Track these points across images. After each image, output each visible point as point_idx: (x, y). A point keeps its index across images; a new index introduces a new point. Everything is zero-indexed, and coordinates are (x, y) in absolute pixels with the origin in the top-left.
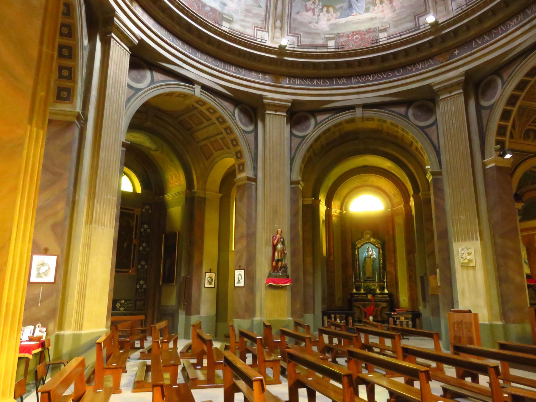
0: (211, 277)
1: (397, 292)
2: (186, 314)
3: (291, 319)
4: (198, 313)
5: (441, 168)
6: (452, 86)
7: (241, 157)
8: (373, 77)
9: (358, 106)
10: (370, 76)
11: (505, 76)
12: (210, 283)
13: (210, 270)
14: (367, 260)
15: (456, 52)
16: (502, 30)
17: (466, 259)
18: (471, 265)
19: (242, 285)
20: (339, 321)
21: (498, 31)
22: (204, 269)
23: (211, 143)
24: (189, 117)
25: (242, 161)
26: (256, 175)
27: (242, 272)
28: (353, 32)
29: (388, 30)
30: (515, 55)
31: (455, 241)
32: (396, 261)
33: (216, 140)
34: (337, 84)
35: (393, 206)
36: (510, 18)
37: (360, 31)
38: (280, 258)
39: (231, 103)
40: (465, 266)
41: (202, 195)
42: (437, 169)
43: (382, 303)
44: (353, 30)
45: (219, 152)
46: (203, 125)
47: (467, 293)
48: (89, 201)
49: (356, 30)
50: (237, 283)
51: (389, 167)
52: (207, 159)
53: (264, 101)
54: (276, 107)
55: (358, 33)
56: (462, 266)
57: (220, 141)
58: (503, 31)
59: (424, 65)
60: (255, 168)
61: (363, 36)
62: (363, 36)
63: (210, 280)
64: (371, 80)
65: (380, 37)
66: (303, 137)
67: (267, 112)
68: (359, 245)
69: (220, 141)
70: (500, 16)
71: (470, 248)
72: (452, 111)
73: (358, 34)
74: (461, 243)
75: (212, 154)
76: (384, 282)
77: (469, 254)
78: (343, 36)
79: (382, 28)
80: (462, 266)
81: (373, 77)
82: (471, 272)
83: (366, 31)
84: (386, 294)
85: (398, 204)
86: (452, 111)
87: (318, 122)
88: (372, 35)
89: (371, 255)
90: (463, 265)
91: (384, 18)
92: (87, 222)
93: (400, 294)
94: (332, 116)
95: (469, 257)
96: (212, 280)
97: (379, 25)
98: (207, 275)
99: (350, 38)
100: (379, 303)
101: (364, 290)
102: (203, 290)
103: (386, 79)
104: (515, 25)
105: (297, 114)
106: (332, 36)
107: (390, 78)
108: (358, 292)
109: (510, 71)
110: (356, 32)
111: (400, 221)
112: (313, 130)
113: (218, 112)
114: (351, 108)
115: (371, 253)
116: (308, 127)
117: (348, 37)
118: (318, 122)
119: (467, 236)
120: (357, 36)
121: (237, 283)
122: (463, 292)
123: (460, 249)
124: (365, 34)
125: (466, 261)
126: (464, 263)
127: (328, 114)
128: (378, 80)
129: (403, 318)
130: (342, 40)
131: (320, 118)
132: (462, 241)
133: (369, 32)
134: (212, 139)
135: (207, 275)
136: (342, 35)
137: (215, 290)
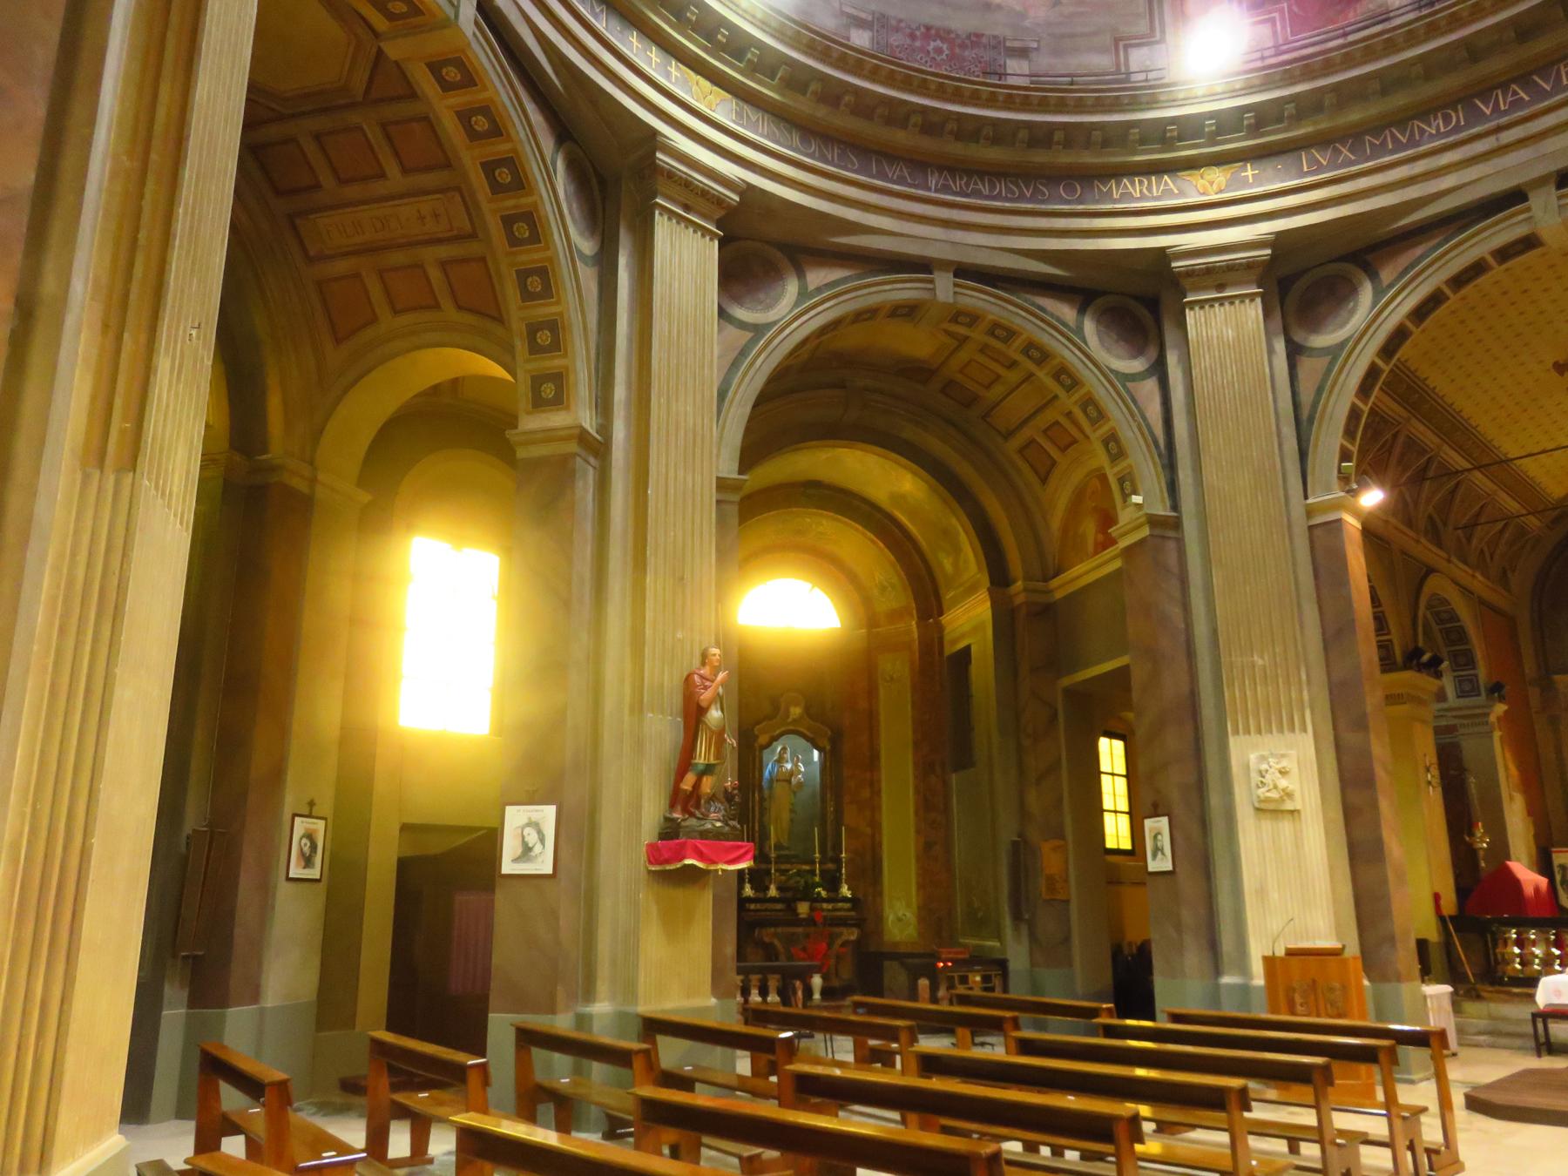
0: (310, 836)
1: (879, 894)
2: (194, 1002)
3: (713, 1001)
4: (254, 995)
5: (1175, 506)
6: (1231, 268)
7: (556, 346)
8: (993, 187)
9: (944, 265)
10: (983, 181)
11: (1386, 275)
12: (308, 861)
13: (311, 804)
14: (779, 789)
15: (1249, 173)
16: (1395, 139)
17: (1275, 787)
18: (1289, 806)
19: (543, 864)
20: (759, 999)
21: (1384, 143)
22: (290, 802)
23: (381, 274)
24: (318, 137)
25: (557, 362)
26: (606, 429)
27: (547, 814)
28: (928, 28)
29: (1033, 55)
30: (1436, 215)
31: (1236, 732)
32: (877, 793)
33: (420, 266)
34: (882, 175)
35: (871, 622)
36: (1425, 112)
37: (949, 32)
38: (712, 761)
39: (547, 119)
40: (1270, 810)
41: (298, 483)
42: (1161, 509)
43: (844, 930)
44: (927, 20)
45: (406, 319)
46: (380, 188)
47: (1274, 896)
48: (113, 328)
49: (938, 23)
50: (516, 860)
51: (899, 499)
52: (338, 341)
53: (1174, 265)
54: (1218, 276)
55: (944, 34)
56: (1258, 810)
57: (435, 274)
58: (1399, 147)
59: (1149, 189)
60: (604, 406)
61: (957, 50)
62: (957, 50)
63: (306, 849)
64: (986, 192)
65: (1009, 71)
66: (758, 330)
67: (658, 200)
68: (763, 739)
69: (435, 274)
70: (1399, 100)
71: (1283, 756)
72: (1226, 334)
73: (943, 39)
74: (1254, 737)
75: (374, 320)
76: (813, 862)
77: (1283, 773)
78: (897, 30)
79: (1016, 44)
80: (1258, 810)
81: (993, 187)
82: (1286, 826)
83: (969, 37)
84: (845, 899)
85: (894, 616)
86: (1226, 334)
87: (811, 287)
88: (987, 56)
89: (791, 773)
90: (1263, 806)
91: (1023, 16)
92: (95, 455)
93: (886, 899)
94: (859, 277)
95: (1283, 783)
96: (314, 847)
97: (1008, 33)
98: (301, 825)
99: (918, 44)
100: (836, 930)
101: (779, 889)
102: (283, 890)
103: (1030, 201)
104: (1439, 135)
105: (756, 245)
106: (863, 15)
107: (1043, 202)
108: (761, 895)
109: (1404, 260)
110: (938, 30)
111: (897, 669)
112: (792, 310)
113: (509, 139)
114: (921, 266)
115: (789, 766)
116: (777, 300)
117: (913, 36)
118: (811, 287)
119: (1278, 719)
120: (938, 43)
121: (516, 860)
122: (1262, 892)
123: (1253, 757)
124: (963, 46)
125: (1274, 795)
126: (1268, 800)
127: (842, 266)
128: (1007, 199)
129: (978, 978)
130: (896, 39)
131: (817, 277)
132: (1259, 732)
133: (975, 45)
134: (398, 258)
135: (301, 825)
136: (894, 23)
137: (323, 886)
